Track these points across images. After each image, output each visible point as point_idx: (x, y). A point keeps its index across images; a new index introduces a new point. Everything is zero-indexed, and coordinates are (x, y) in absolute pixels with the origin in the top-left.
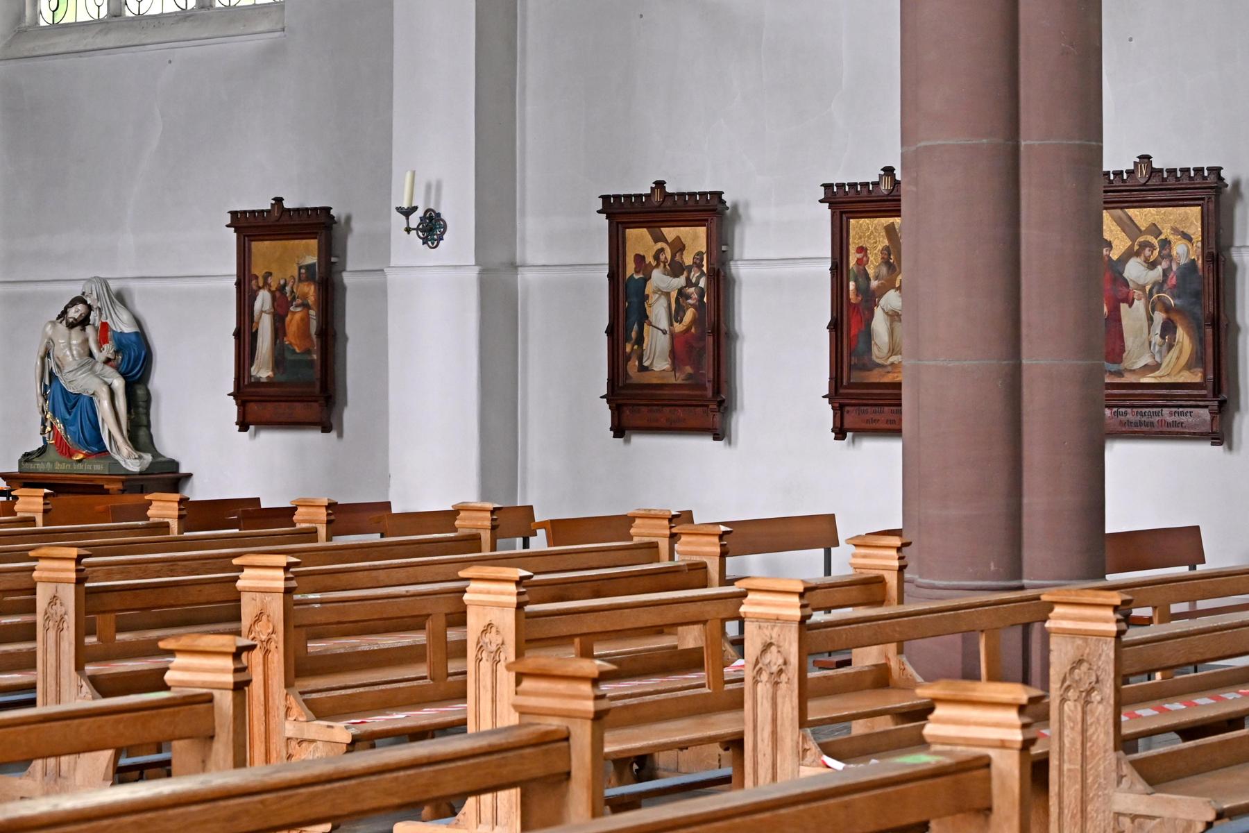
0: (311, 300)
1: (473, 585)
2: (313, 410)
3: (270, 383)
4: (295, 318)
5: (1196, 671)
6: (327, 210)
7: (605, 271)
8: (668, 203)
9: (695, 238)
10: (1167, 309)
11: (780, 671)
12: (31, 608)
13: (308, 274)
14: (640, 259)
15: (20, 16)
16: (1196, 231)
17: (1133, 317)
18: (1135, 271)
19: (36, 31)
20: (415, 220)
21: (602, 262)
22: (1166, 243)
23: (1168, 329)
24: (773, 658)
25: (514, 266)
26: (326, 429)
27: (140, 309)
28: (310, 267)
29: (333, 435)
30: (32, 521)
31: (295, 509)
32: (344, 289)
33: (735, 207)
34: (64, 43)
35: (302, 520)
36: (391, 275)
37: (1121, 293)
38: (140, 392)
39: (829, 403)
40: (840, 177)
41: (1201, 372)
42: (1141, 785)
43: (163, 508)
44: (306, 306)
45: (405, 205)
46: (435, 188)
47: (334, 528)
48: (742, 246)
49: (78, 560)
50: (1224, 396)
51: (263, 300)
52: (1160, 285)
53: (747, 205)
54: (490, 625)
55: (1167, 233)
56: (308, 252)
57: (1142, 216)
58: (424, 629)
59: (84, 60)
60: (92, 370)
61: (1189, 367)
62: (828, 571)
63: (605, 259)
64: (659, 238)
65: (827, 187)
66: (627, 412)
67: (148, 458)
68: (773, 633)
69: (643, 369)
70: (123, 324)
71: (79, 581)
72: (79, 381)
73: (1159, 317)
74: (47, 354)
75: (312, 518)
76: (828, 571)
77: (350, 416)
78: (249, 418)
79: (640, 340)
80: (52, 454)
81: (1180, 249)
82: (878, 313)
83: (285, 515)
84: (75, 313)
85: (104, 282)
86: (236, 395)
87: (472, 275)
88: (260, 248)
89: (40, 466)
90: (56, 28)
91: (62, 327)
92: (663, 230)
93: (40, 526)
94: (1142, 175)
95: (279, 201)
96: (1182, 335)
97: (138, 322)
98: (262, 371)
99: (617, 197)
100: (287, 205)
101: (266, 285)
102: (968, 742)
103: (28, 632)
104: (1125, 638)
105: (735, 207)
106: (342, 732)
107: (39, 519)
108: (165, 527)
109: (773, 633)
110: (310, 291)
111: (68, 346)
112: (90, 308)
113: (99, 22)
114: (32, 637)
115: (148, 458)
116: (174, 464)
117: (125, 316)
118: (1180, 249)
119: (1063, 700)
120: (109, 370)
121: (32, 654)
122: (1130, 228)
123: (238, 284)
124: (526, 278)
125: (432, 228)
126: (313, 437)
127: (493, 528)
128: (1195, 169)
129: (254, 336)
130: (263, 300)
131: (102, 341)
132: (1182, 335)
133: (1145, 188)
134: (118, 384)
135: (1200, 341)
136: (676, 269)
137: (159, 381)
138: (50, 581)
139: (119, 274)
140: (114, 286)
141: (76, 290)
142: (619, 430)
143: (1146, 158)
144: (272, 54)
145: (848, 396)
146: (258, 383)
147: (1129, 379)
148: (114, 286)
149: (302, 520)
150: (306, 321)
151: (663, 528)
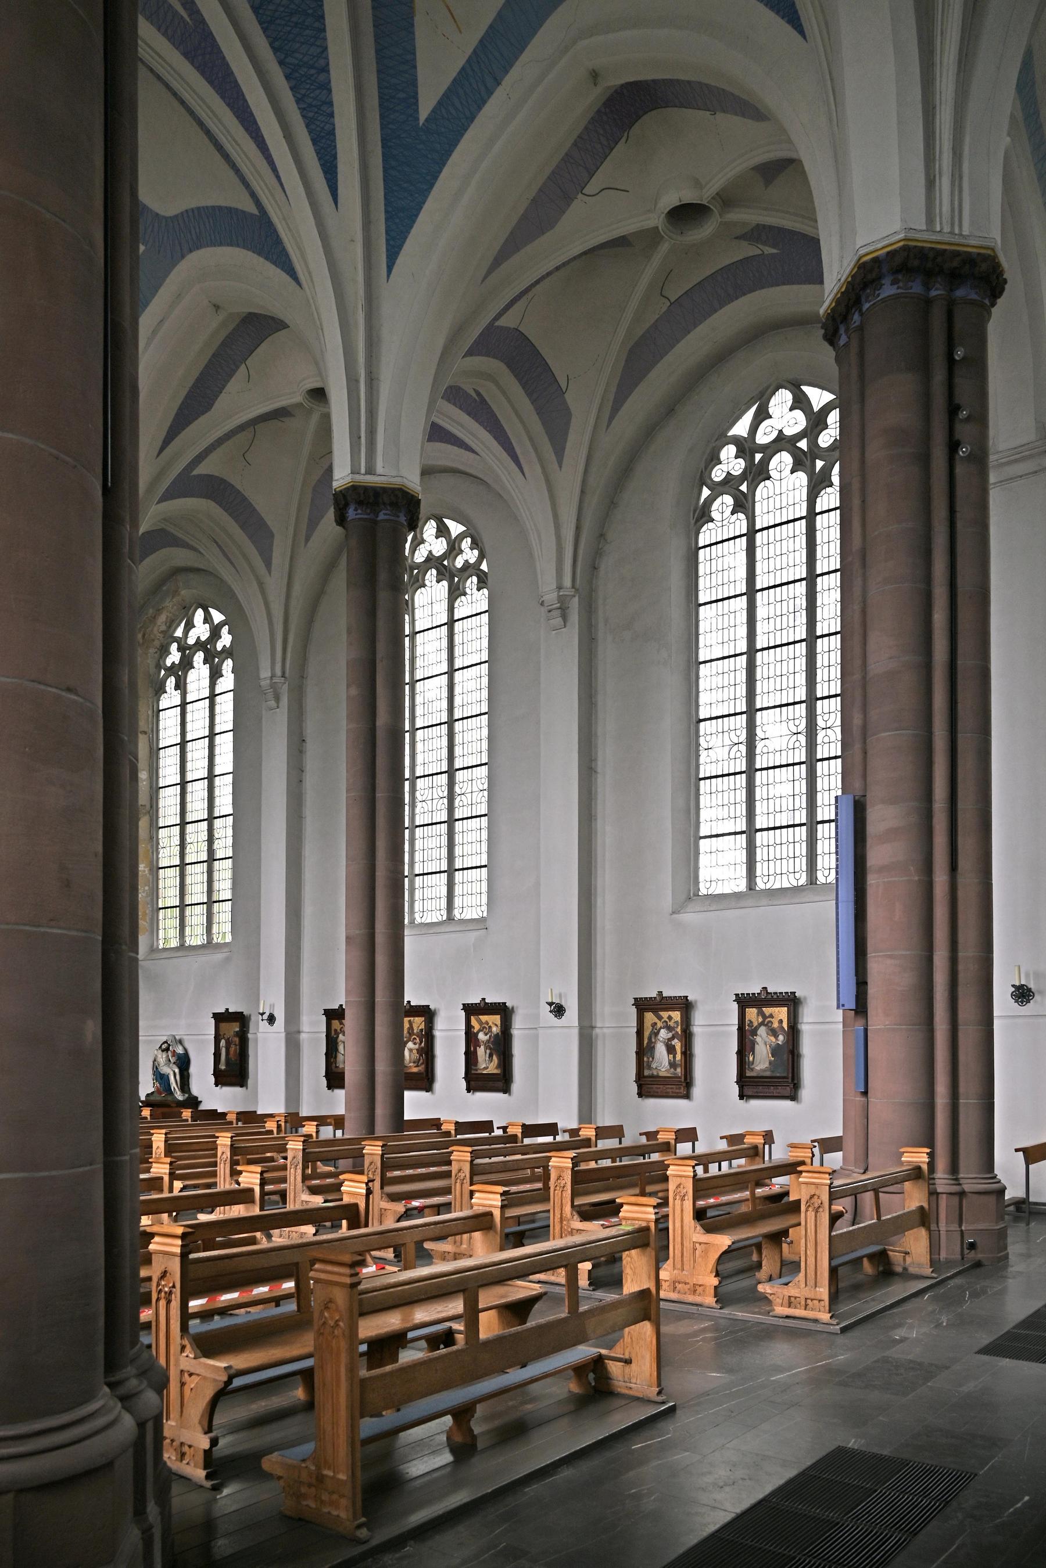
0: (237, 1043)
1: (367, 1147)
3: (225, 1071)
4: (232, 1049)
9: (781, 1013)
10: (490, 1049)
11: (819, 1207)
12: (215, 1156)
13: (237, 1034)
14: (336, 1030)
15: (152, 945)
16: (499, 1023)
17: (481, 1051)
18: (481, 1036)
19: (158, 950)
20: (265, 1017)
22: (490, 1027)
23: (491, 1056)
24: (224, 1156)
25: (299, 1032)
26: (242, 1086)
27: (187, 1045)
28: (237, 1032)
29: (244, 1088)
30: (187, 1120)
31: (745, 1135)
32: (248, 1039)
33: (435, 1010)
34: (165, 955)
35: (229, 1118)
36: (259, 1035)
37: (477, 1043)
38: (186, 1073)
39: (737, 1082)
42: (702, 1231)
43: (187, 1114)
44: (235, 1045)
46: (272, 1006)
47: (457, 1133)
48: (802, 1017)
49: (232, 1137)
50: (796, 1082)
51: (223, 1043)
52: (488, 1041)
53: (517, 1007)
54: (680, 1184)
55: (490, 1024)
56: (236, 1027)
57: (484, 1018)
59: (171, 961)
60: (169, 1066)
61: (497, 1068)
62: (694, 1151)
63: (325, 1030)
64: (660, 1018)
65: (737, 995)
67: (187, 1095)
68: (224, 1149)
69: (336, 1067)
70: (180, 1050)
71: (166, 1141)
72: (165, 1070)
73: (488, 1051)
74: (155, 1060)
75: (231, 1117)
76: (694, 1151)
77: (250, 1082)
78: (643, 1093)
79: (336, 1057)
80: (155, 1094)
81: (494, 1029)
82: (406, 1049)
83: (224, 1115)
84: (164, 1047)
85: (174, 1036)
86: (214, 1074)
87: (283, 1035)
88: (223, 1026)
89: (152, 1098)
90: (164, 949)
91: (160, 1051)
92: (764, 1009)
93: (190, 1122)
94: (482, 1005)
95: (227, 1009)
96: (495, 1057)
97: (185, 1049)
98: (222, 1067)
100: (230, 1011)
101: (224, 1038)
102: (159, 1173)
103: (215, 1164)
104: (475, 1162)
105: (435, 1010)
106: (400, 1207)
107: (190, 1119)
108: (146, 1118)
109: (224, 1149)
110: (237, 1040)
111: (162, 1058)
112: (169, 1045)
113: (177, 947)
114: (216, 1166)
115: (187, 1095)
116: (197, 1098)
117: (181, 1048)
118: (494, 1029)
119: (807, 1211)
120: (174, 1066)
121: (216, 1171)
122: (480, 1022)
124: (303, 1036)
125: (271, 1019)
126: (237, 1090)
127: (596, 1135)
129: (220, 1055)
130: (223, 1043)
131: (173, 1056)
132: (495, 1057)
133: (482, 1009)
134: (177, 1070)
135: (499, 1059)
136: (669, 1028)
137: (192, 1070)
138: (293, 1149)
139: (179, 1034)
140: (178, 1038)
141: (164, 1039)
143: (765, 988)
144: (228, 960)
145: (745, 1082)
146: (221, 1070)
147: (479, 1072)
148: (178, 1038)
149: (229, 1118)
150: (236, 1050)
151: (760, 1140)
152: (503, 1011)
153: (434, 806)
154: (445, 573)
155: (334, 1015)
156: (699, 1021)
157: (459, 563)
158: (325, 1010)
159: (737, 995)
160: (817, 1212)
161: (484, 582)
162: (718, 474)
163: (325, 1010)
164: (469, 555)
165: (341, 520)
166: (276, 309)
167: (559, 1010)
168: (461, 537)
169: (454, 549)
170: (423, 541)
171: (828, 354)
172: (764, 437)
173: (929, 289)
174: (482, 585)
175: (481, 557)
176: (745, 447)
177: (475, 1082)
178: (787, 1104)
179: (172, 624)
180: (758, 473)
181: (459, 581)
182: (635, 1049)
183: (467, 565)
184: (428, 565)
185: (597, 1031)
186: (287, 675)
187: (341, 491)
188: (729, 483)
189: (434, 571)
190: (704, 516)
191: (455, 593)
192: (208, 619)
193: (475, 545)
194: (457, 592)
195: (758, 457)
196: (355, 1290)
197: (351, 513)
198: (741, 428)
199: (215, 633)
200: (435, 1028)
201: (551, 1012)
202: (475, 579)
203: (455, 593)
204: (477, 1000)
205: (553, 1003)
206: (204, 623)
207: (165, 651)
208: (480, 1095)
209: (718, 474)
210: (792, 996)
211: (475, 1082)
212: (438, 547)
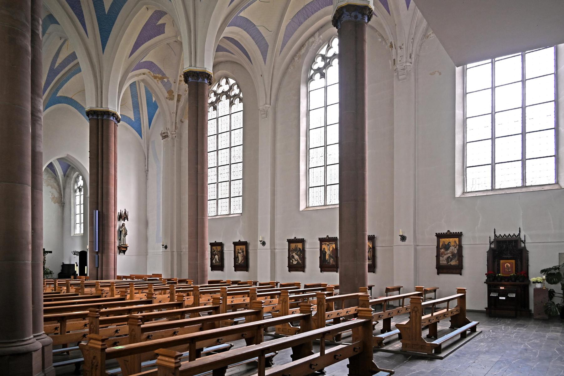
2: (335, 269)
5: (277, 288)
6: (222, 243)
7: (288, 250)
8: (329, 239)
20: (164, 246)
21: (260, 250)
26: (247, 271)
32: (249, 252)
40: (320, 237)
41: (214, 263)
45: (261, 240)
56: (219, 248)
58: (208, 281)
66: (322, 269)
99: (289, 239)
123: (211, 252)
125: (264, 244)
126: (245, 272)
128: (460, 232)
133: (328, 240)
142: (438, 274)
152: (245, 244)
153: (213, 177)
154: (228, 97)
155: (123, 249)
156: (225, 249)
157: (233, 94)
158: (210, 243)
159: (436, 234)
160: (285, 303)
161: (241, 100)
162: (315, 67)
163: (210, 243)
164: (236, 91)
165: (186, 81)
166: (165, 9)
167: (264, 244)
168: (233, 85)
169: (231, 88)
170: (332, 47)
171: (335, 30)
172: (330, 54)
173: (98, 117)
174: (241, 101)
175: (240, 91)
176: (324, 58)
177: (238, 267)
178: (301, 273)
179: (320, 47)
180: (218, 100)
181: (233, 100)
182: (210, 257)
183: (235, 95)
184: (223, 94)
185: (276, 250)
186: (271, 104)
187: (186, 72)
188: (319, 70)
189: (225, 96)
190: (311, 79)
191: (231, 104)
192: (227, 83)
193: (238, 87)
194: (232, 104)
195: (328, 60)
196: (97, 319)
197: (190, 79)
198: (323, 52)
199: (231, 88)
200: (306, 247)
201: (261, 244)
202: (238, 99)
203: (231, 104)
204: (214, 242)
205: (262, 241)
206: (226, 84)
207: (313, 61)
208: (326, 273)
209: (315, 67)
210: (374, 236)
211: (238, 267)
212: (226, 88)
